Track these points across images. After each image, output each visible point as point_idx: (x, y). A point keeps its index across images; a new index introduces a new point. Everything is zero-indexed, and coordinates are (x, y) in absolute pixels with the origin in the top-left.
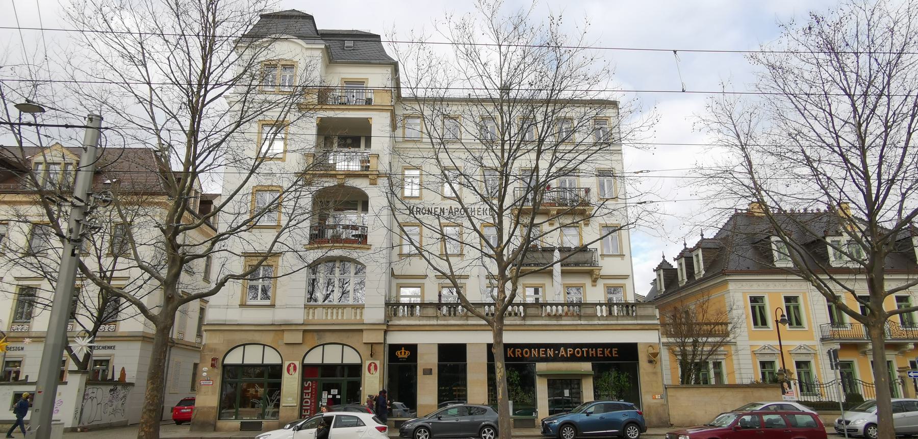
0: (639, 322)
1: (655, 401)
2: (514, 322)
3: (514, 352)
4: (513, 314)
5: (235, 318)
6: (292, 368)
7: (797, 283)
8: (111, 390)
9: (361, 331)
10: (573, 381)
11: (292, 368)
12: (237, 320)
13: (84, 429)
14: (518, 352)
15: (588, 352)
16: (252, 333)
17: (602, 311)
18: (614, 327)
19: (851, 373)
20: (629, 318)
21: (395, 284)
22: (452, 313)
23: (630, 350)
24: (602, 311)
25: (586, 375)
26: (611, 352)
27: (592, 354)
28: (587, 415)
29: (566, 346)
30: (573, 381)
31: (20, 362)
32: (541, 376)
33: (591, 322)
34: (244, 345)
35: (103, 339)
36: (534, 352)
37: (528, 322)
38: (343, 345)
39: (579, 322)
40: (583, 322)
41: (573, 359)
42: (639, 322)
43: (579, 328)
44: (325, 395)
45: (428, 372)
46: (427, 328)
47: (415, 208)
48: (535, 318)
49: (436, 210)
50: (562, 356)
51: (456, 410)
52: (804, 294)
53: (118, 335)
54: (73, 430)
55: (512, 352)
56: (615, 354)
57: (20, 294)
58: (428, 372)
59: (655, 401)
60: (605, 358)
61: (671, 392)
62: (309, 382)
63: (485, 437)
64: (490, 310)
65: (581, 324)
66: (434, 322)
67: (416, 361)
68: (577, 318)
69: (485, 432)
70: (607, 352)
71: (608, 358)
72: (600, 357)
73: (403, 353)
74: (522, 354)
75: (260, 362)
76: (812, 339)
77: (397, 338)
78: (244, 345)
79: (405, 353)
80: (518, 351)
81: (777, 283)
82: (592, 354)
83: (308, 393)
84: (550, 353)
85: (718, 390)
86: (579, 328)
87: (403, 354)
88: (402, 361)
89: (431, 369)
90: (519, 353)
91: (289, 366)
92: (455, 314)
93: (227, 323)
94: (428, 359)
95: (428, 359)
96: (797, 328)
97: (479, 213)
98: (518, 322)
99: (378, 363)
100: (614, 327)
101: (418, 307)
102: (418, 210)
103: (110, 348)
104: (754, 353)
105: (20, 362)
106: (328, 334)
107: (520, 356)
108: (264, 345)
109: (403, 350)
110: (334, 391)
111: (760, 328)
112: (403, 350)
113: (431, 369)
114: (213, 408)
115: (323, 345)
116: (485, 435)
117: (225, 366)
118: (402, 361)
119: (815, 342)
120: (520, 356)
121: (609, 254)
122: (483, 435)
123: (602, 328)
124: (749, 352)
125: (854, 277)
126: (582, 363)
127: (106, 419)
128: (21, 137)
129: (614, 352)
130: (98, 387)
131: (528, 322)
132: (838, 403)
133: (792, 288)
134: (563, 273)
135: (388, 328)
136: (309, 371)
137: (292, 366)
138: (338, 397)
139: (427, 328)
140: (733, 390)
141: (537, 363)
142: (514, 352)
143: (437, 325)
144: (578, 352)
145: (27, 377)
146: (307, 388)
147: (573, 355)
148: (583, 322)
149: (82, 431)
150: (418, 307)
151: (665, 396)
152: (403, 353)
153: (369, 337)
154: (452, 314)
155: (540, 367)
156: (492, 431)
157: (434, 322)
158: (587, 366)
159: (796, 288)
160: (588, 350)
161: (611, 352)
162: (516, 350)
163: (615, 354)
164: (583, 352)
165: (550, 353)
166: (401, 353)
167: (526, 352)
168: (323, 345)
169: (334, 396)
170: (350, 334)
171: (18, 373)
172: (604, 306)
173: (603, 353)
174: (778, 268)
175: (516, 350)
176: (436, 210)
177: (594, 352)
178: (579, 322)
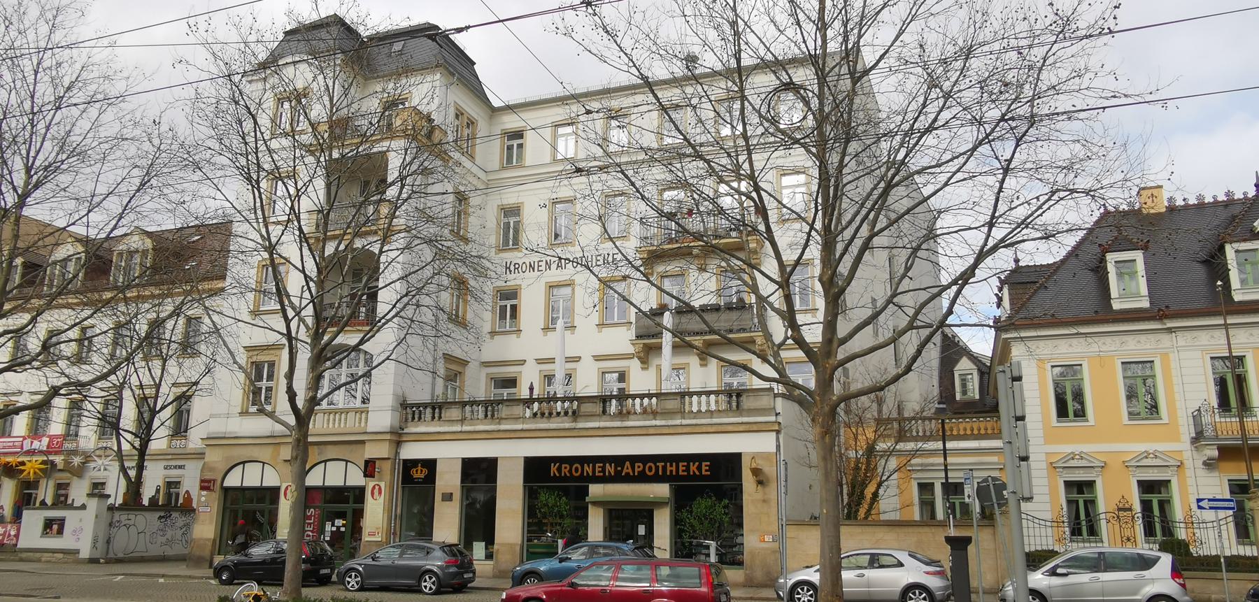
0: (745, 419)
1: (763, 545)
2: (562, 426)
3: (559, 470)
4: (570, 413)
5: (236, 430)
6: (376, 491)
7: (1150, 336)
8: (160, 518)
9: (363, 442)
10: (643, 513)
11: (376, 491)
12: (236, 433)
13: (109, 561)
14: (565, 469)
15: (664, 468)
16: (251, 447)
17: (699, 403)
18: (704, 429)
19: (1094, 501)
20: (730, 414)
21: (485, 375)
22: (437, 415)
23: (728, 465)
24: (699, 403)
25: (660, 504)
26: (699, 468)
27: (671, 471)
28: (560, 562)
29: (633, 459)
30: (643, 513)
31: (104, 483)
32: (595, 503)
33: (671, 422)
34: (244, 463)
35: (174, 457)
36: (588, 469)
37: (580, 425)
38: (347, 461)
39: (654, 423)
40: (658, 423)
41: (642, 478)
42: (745, 419)
43: (652, 431)
44: (328, 527)
45: (448, 497)
46: (448, 437)
47: (513, 264)
48: (592, 418)
49: (599, 258)
50: (628, 474)
51: (869, 557)
52: (1165, 356)
53: (188, 452)
54: (93, 561)
55: (557, 469)
56: (706, 471)
57: (70, 408)
58: (448, 497)
59: (763, 545)
60: (689, 478)
61: (791, 532)
62: (312, 510)
63: (799, 599)
64: (650, 404)
65: (656, 426)
66: (457, 428)
67: (434, 483)
68: (651, 416)
69: (350, 577)
70: (693, 468)
71: (695, 478)
72: (599, 476)
73: (419, 472)
74: (570, 471)
75: (341, 483)
76: (1177, 439)
77: (412, 451)
78: (244, 463)
79: (422, 471)
80: (566, 468)
81: (1143, 338)
82: (671, 471)
83: (310, 524)
84: (627, 468)
85: (926, 529)
86: (652, 431)
87: (419, 474)
88: (418, 483)
89: (452, 494)
90: (567, 470)
91: (374, 487)
92: (493, 416)
93: (227, 436)
94: (449, 480)
95: (449, 480)
96: (1074, 421)
97: (540, 268)
98: (567, 425)
99: (382, 485)
100: (704, 429)
101: (614, 402)
102: (517, 266)
103: (180, 467)
104: (1053, 466)
105: (104, 483)
106: (329, 447)
107: (568, 475)
108: (264, 463)
109: (419, 468)
110: (339, 522)
111: (1071, 421)
112: (419, 468)
113: (452, 494)
114: (209, 540)
115: (325, 461)
116: (425, 584)
117: (226, 490)
118: (418, 483)
119: (1183, 445)
120: (568, 475)
121: (612, 322)
122: (348, 579)
123: (685, 430)
124: (1044, 465)
125: (1222, 322)
126: (655, 485)
127: (155, 551)
128: (693, 147)
129: (704, 468)
130: (137, 513)
131: (580, 425)
132: (1217, 557)
133: (1139, 347)
134: (675, 347)
135: (398, 437)
136: (309, 496)
137: (377, 487)
138: (343, 529)
139: (448, 437)
140: (898, 530)
141: (590, 485)
142: (559, 470)
143: (461, 432)
144: (650, 468)
145: (73, 500)
146: (309, 518)
147: (643, 473)
148: (658, 423)
149: (106, 563)
150: (614, 402)
151: (780, 538)
152: (419, 472)
153: (371, 451)
154: (489, 416)
155: (595, 490)
156: (434, 579)
157: (457, 428)
158: (662, 490)
159: (1079, 350)
160: (666, 465)
161: (699, 468)
162: (563, 466)
163: (706, 471)
164: (657, 468)
165: (610, 469)
166: (417, 471)
167: (577, 469)
168: (325, 461)
169: (338, 528)
170: (353, 447)
171: (66, 496)
172: (654, 398)
173: (688, 469)
174: (1240, 302)
175: (563, 466)
176: (540, 263)
177: (674, 469)
178: (654, 423)
